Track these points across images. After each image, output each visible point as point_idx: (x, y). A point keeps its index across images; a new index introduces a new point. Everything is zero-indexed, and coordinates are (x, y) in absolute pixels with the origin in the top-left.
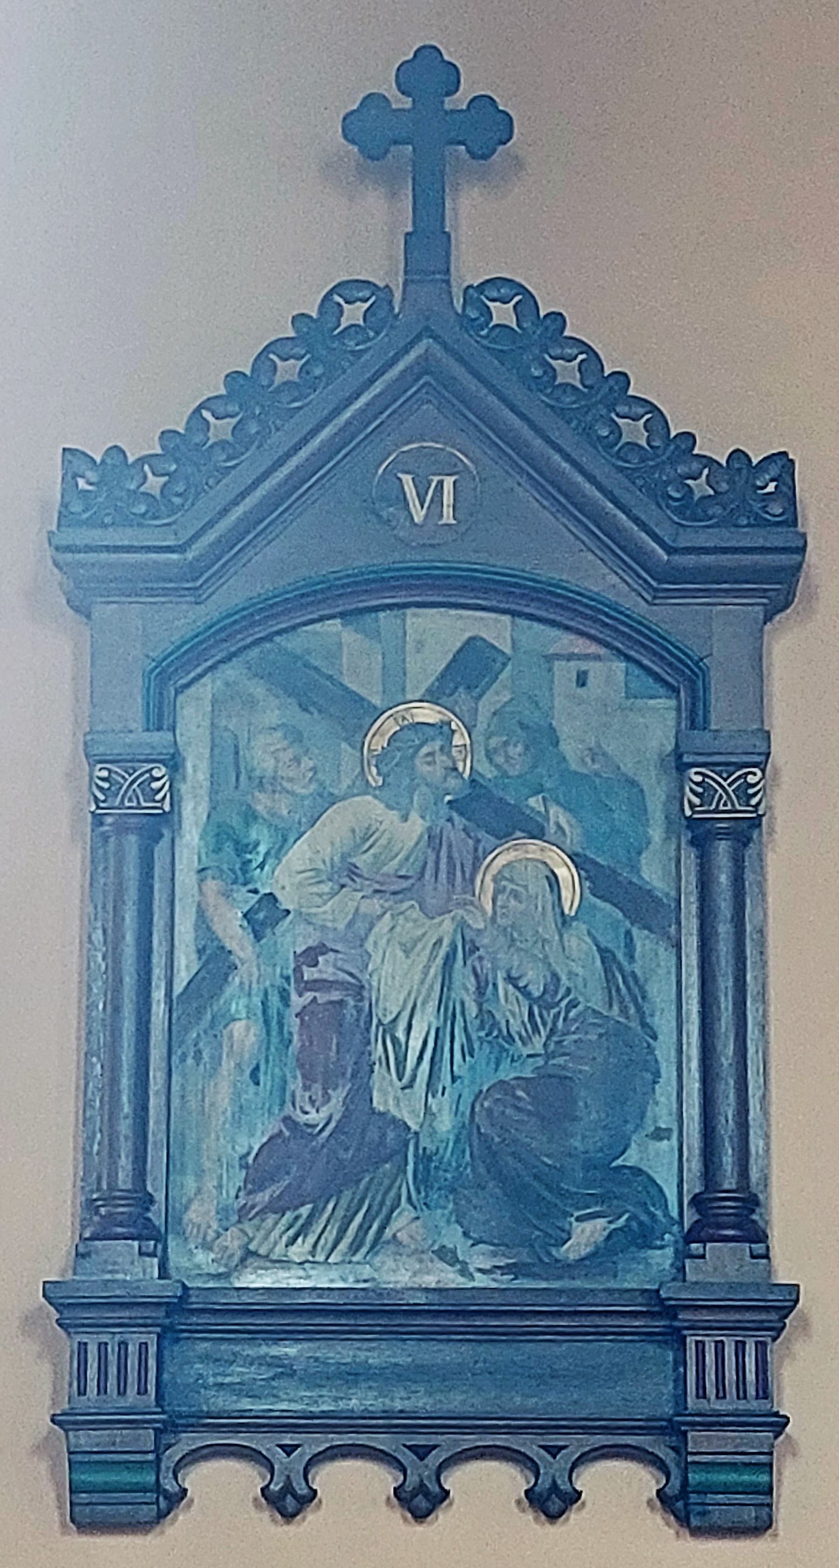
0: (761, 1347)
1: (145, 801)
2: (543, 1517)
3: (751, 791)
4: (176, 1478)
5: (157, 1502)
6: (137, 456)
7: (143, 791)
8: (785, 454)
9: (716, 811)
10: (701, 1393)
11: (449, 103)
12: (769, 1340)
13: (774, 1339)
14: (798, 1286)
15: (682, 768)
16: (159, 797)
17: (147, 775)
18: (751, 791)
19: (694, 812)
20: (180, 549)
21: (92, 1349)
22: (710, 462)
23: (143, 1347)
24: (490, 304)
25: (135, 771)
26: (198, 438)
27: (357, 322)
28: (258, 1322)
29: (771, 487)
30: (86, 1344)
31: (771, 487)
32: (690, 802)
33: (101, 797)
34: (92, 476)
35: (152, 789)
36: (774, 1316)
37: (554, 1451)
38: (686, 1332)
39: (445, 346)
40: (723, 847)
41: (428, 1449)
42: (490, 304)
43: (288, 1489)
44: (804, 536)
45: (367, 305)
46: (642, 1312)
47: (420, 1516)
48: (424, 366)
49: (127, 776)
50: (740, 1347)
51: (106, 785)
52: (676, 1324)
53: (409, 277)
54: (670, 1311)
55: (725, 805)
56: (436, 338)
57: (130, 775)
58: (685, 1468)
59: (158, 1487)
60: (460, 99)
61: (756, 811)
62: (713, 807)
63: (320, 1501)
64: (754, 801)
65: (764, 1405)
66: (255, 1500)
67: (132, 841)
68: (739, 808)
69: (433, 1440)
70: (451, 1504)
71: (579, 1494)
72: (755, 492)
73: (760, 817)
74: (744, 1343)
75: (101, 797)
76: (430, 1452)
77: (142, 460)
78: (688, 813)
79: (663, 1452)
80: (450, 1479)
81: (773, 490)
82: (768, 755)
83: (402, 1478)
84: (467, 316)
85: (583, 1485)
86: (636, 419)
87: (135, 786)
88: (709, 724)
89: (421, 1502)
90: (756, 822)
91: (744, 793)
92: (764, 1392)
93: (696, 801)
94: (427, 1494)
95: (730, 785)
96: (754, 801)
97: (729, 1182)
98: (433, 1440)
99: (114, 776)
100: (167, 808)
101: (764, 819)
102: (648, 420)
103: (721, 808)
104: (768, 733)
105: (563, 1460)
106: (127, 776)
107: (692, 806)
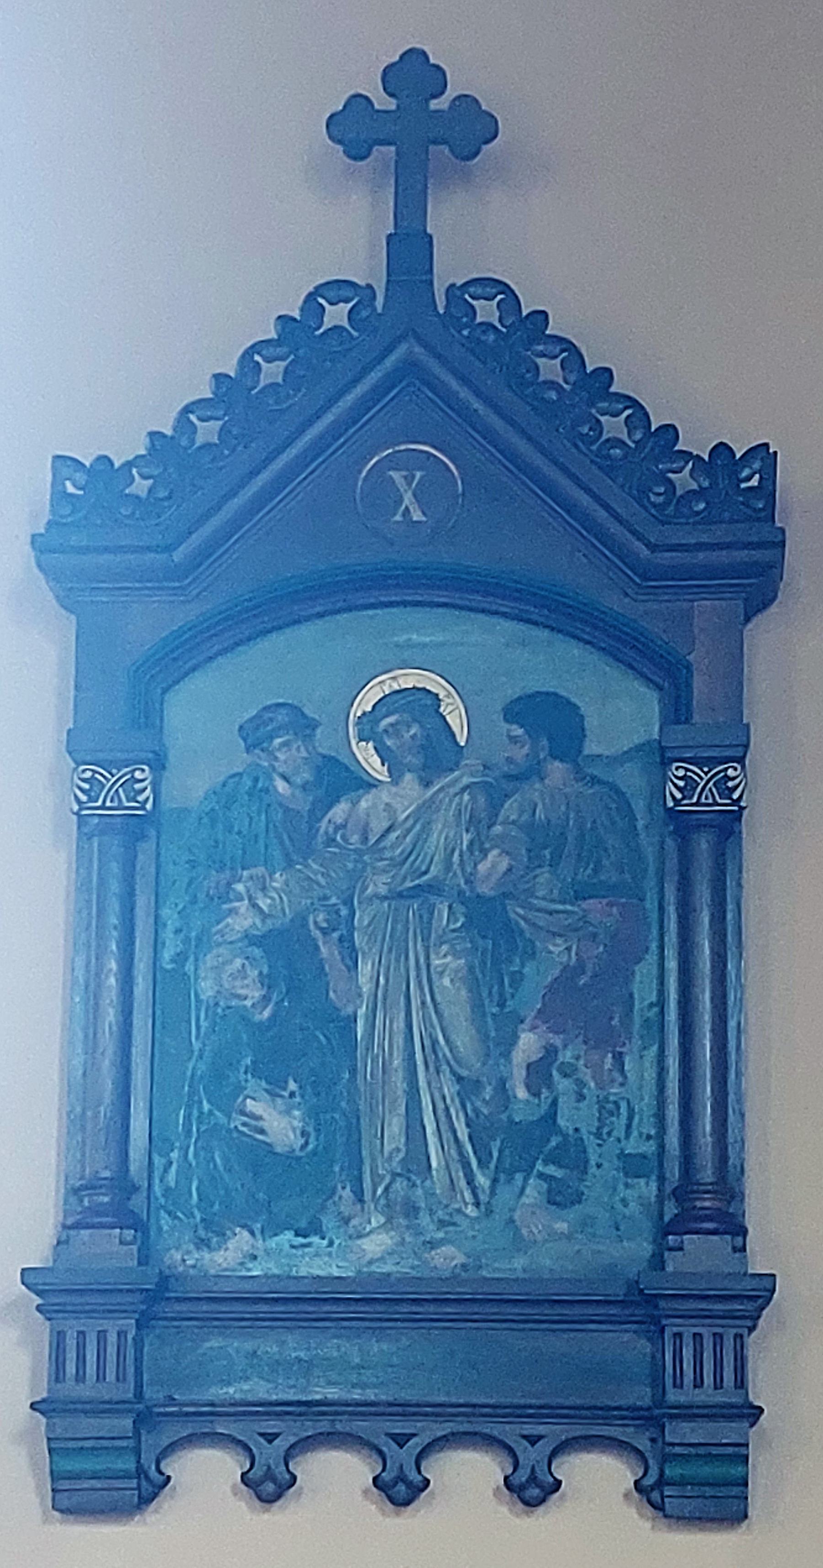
0: (739, 1337)
1: (128, 801)
2: (520, 1505)
3: (730, 784)
4: (419, 1472)
5: (139, 1488)
6: (684, 449)
7: (717, 789)
8: (766, 445)
9: (697, 804)
10: (678, 1384)
11: (434, 104)
12: (746, 1330)
13: (751, 1329)
14: (774, 1275)
15: (666, 763)
16: (141, 798)
17: (722, 774)
18: (138, 786)
19: (675, 805)
20: (653, 548)
21: (112, 1338)
22: (687, 455)
23: (121, 1334)
24: (474, 303)
25: (119, 771)
26: (184, 442)
27: (340, 323)
28: (224, 1309)
29: (754, 482)
30: (105, 1331)
31: (754, 482)
32: (673, 797)
33: (84, 798)
34: (81, 477)
35: (728, 788)
36: (749, 1306)
37: (401, 1440)
38: (664, 1322)
39: (426, 346)
40: (703, 844)
41: (406, 1438)
42: (474, 303)
43: (533, 1479)
44: (782, 531)
45: (350, 305)
46: (600, 1301)
47: (268, 1500)
48: (410, 366)
49: (702, 775)
50: (718, 1338)
51: (681, 783)
52: (656, 1313)
53: (429, 276)
54: (652, 1300)
55: (706, 798)
56: (419, 339)
57: (706, 773)
58: (665, 1459)
59: (141, 1472)
60: (382, 101)
61: (143, 808)
62: (99, 803)
63: (301, 1488)
64: (735, 796)
65: (728, 1396)
66: (234, 1487)
67: (115, 845)
68: (720, 801)
69: (541, 1429)
70: (299, 1494)
71: (559, 1483)
72: (738, 486)
73: (742, 809)
74: (721, 1336)
75: (84, 798)
76: (408, 1441)
77: (129, 464)
78: (670, 804)
79: (643, 1443)
80: (566, 1467)
81: (756, 484)
82: (746, 746)
83: (248, 1466)
84: (452, 316)
85: (174, 1470)
86: (616, 415)
87: (711, 783)
88: (692, 717)
89: (270, 1487)
90: (737, 816)
91: (724, 788)
92: (741, 1383)
93: (679, 796)
94: (409, 1484)
95: (701, 779)
96: (735, 796)
97: (707, 1175)
98: (541, 1429)
99: (97, 776)
100: (149, 806)
101: (745, 813)
102: (628, 417)
103: (108, 804)
104: (748, 726)
105: (544, 1448)
106: (702, 775)
107: (673, 797)
